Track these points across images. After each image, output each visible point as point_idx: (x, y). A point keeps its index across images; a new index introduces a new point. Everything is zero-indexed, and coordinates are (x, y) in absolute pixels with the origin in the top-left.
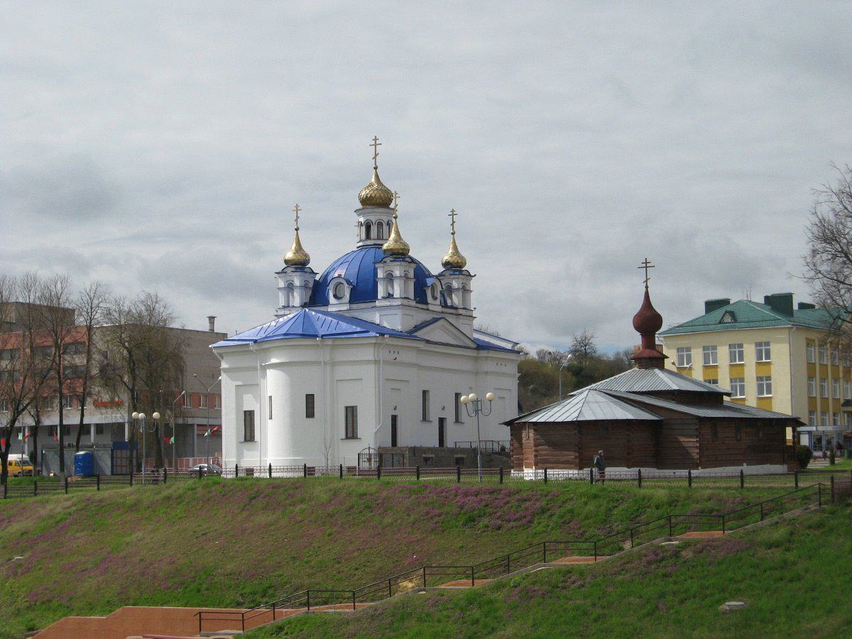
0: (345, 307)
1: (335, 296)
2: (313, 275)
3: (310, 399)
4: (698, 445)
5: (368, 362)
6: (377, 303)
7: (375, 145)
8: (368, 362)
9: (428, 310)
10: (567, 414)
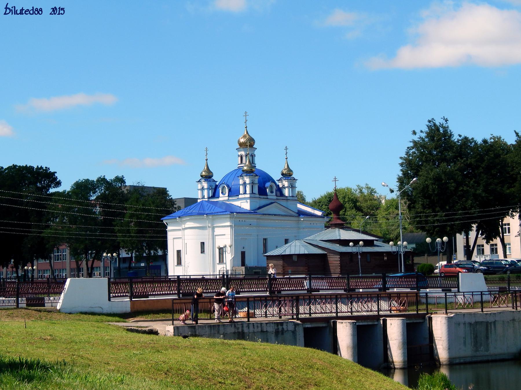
0: (227, 198)
1: (222, 193)
2: (214, 182)
3: (203, 244)
4: (340, 265)
5: (227, 226)
6: (240, 196)
7: (246, 116)
8: (227, 226)
9: (268, 198)
10: (274, 253)
